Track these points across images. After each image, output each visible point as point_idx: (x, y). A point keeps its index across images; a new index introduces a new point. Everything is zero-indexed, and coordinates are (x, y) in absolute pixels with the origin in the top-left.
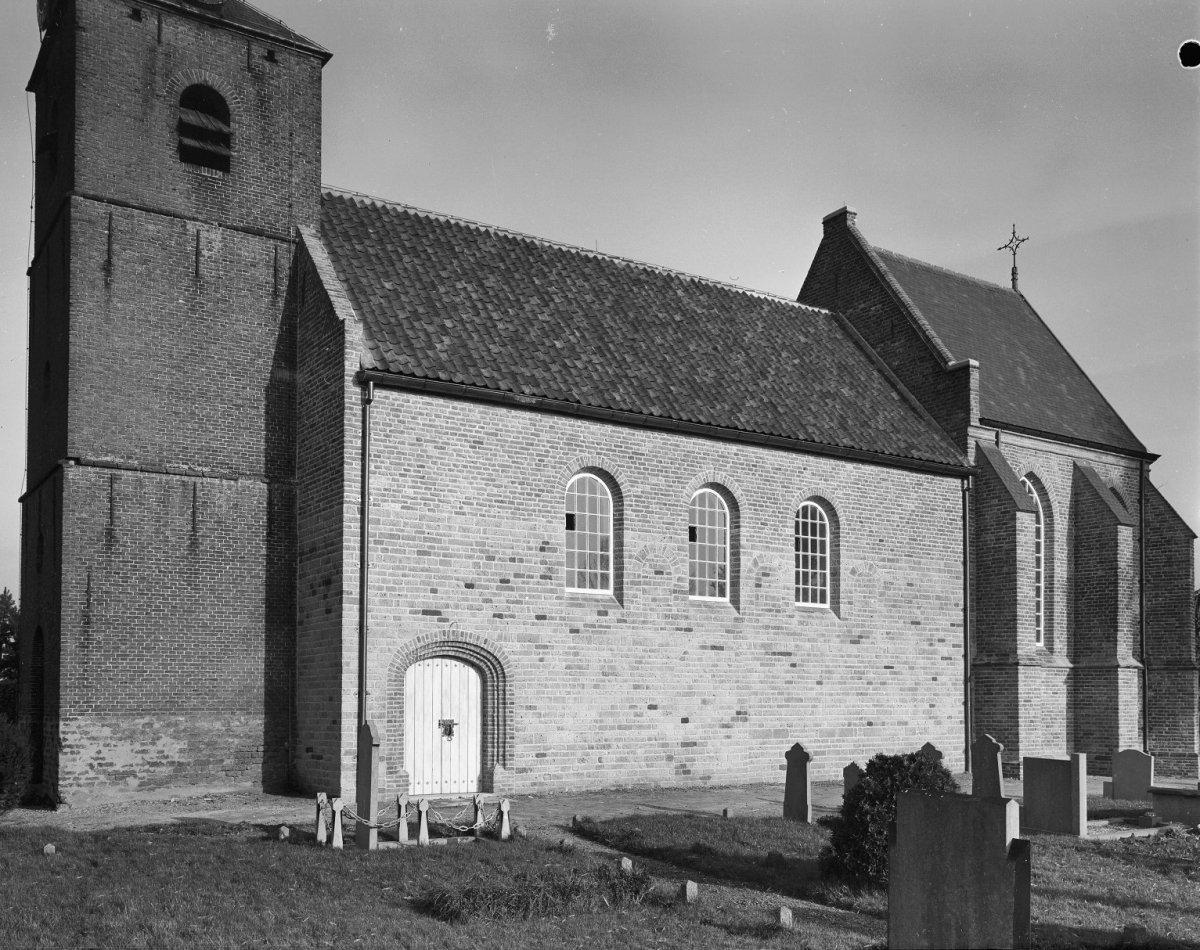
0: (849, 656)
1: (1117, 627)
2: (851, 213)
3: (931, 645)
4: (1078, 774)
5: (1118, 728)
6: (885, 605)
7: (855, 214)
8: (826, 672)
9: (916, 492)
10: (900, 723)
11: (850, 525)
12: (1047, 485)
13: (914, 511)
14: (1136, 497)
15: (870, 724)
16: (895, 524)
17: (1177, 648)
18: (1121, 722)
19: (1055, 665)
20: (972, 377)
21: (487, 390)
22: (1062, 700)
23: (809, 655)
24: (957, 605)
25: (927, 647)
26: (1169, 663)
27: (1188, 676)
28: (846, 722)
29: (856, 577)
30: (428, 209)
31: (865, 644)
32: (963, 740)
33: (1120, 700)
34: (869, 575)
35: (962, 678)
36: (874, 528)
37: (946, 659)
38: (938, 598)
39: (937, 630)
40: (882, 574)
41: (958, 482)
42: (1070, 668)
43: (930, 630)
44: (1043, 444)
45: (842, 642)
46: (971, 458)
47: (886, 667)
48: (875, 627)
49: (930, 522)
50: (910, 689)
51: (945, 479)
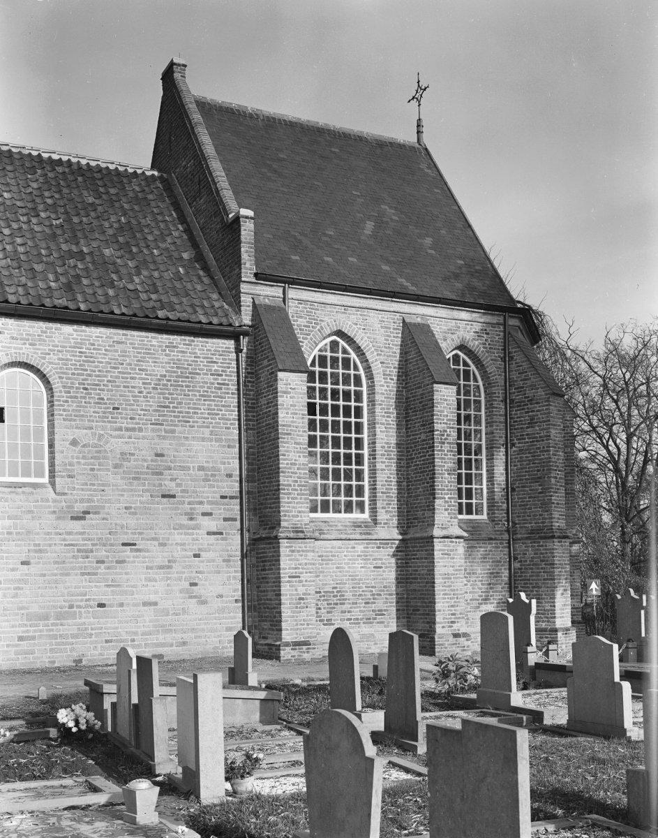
0: (69, 533)
1: (434, 494)
2: (179, 65)
3: (191, 519)
4: (413, 654)
5: (435, 603)
6: (122, 478)
7: (185, 66)
8: (36, 551)
9: (166, 355)
10: (145, 604)
11: (69, 392)
12: (363, 345)
13: (165, 376)
14: (497, 354)
15: (101, 605)
16: (136, 390)
17: (540, 515)
18: (439, 597)
19: (374, 537)
20: (242, 228)
21: (222, 328)
22: (391, 575)
23: (9, 533)
24: (230, 476)
25: (186, 522)
26: (532, 532)
27: (549, 545)
28: (67, 604)
29: (78, 449)
30: (21, 144)
31: (92, 520)
32: (241, 620)
33: (436, 572)
34: (96, 446)
35: (239, 553)
36: (105, 395)
37: (214, 533)
38: (201, 468)
39: (201, 503)
40: (117, 445)
41: (230, 344)
42: (400, 540)
43: (189, 503)
44: (355, 299)
45: (59, 518)
46: (246, 319)
47: (124, 544)
48: (109, 501)
49: (187, 386)
50: (161, 567)
51: (210, 340)
